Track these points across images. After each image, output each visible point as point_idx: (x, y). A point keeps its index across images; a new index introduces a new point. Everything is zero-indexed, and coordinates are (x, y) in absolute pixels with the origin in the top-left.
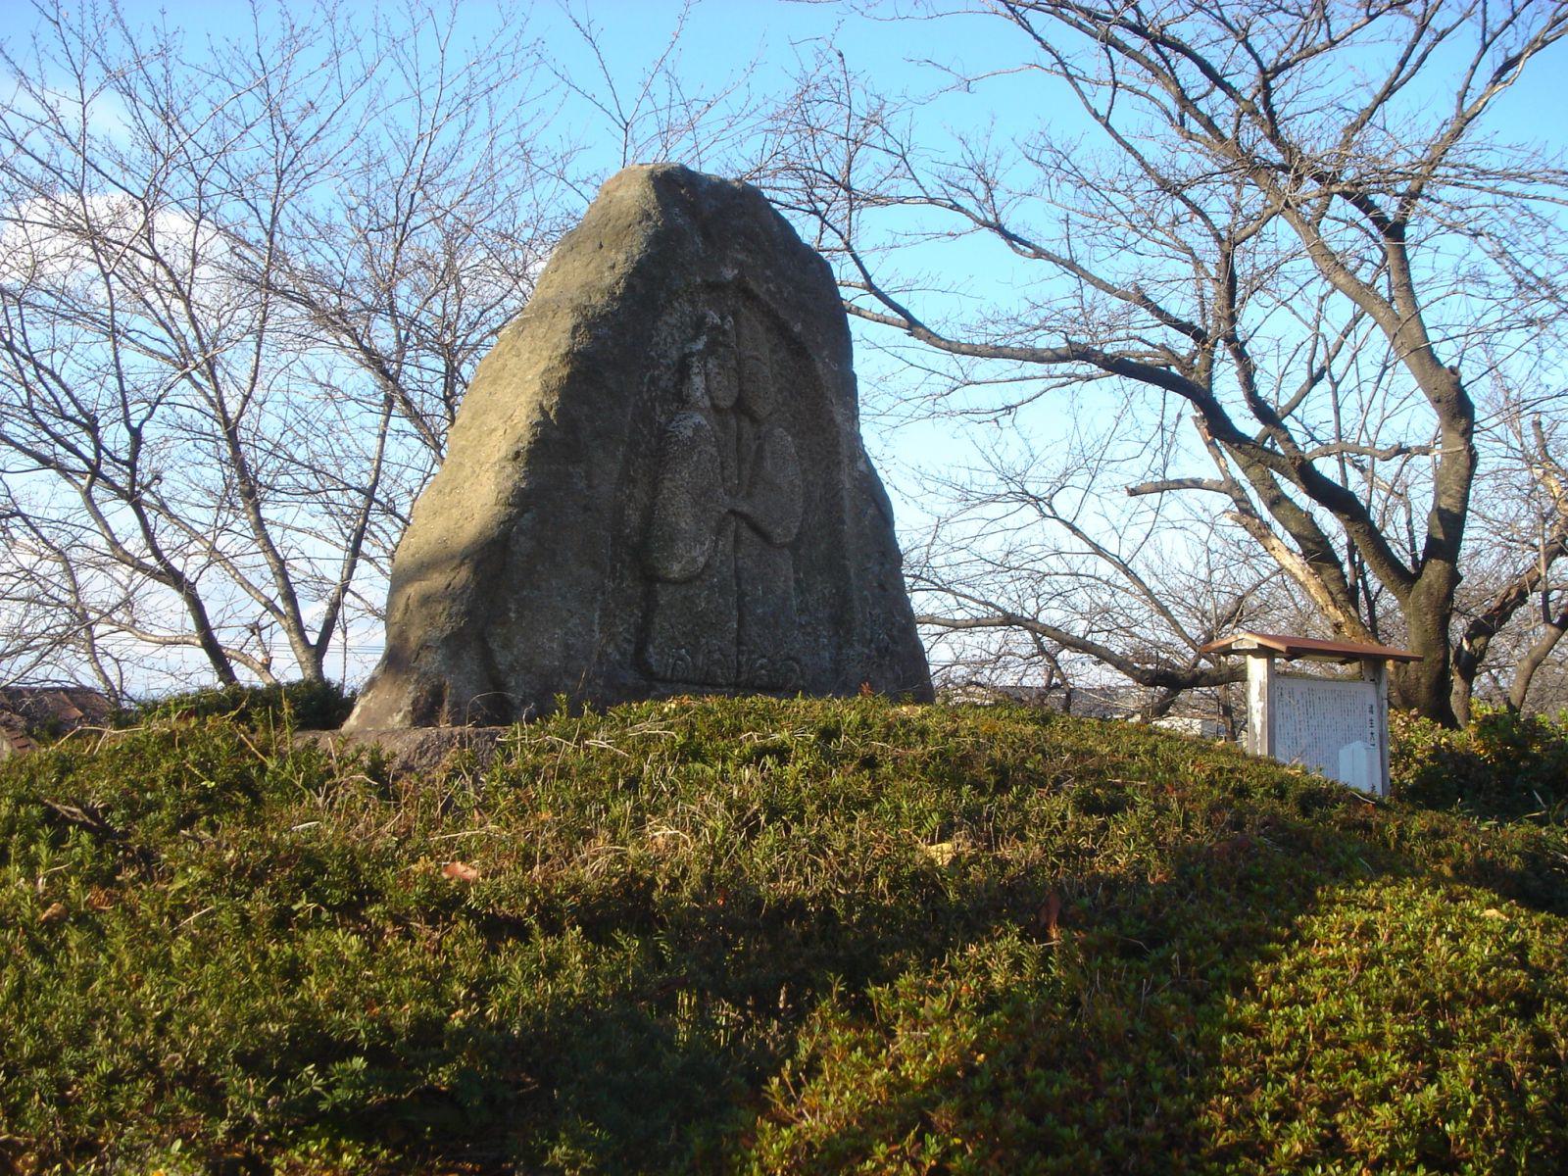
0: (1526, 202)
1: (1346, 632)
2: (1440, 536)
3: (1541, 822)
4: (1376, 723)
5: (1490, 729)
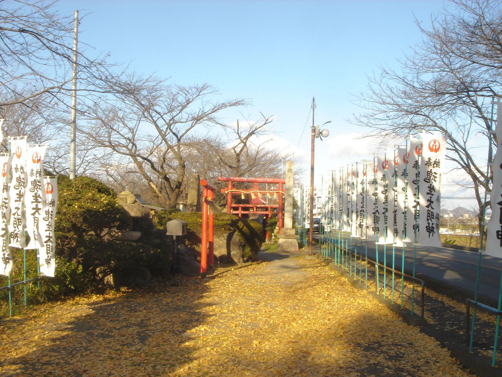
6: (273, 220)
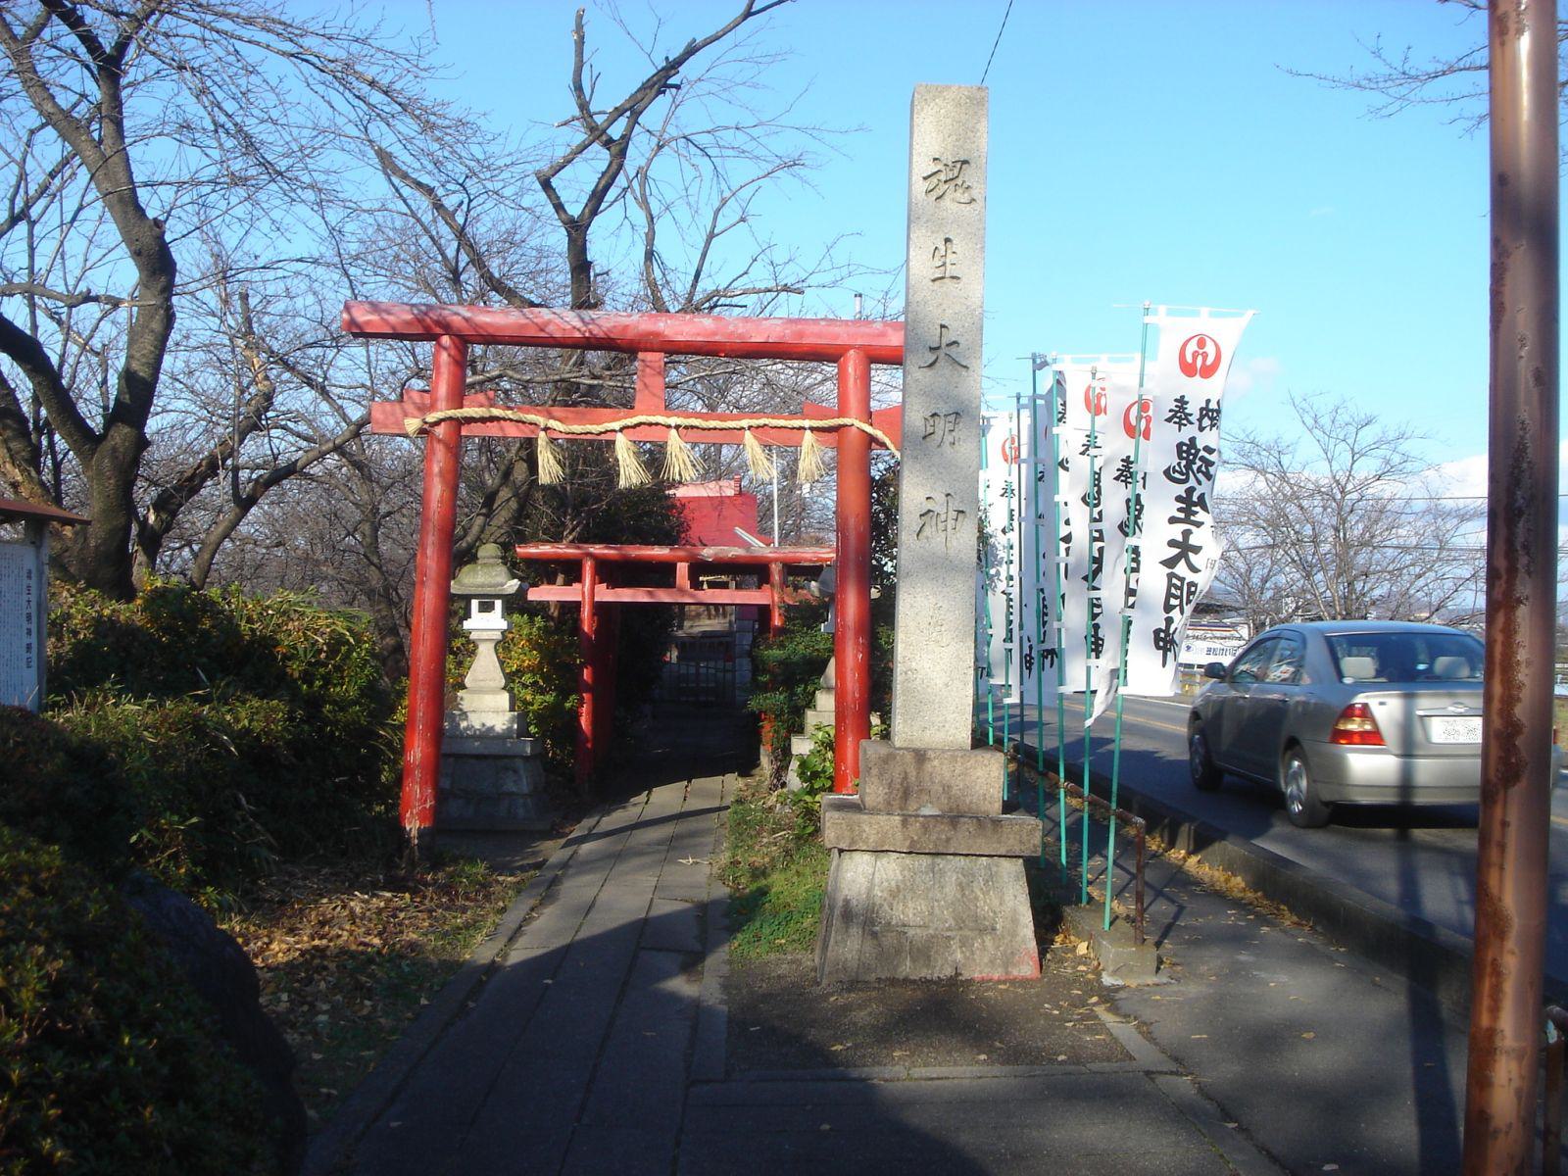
0: (239, 45)
1: (24, 492)
2: (127, 398)
3: (203, 700)
4: (34, 591)
5: (160, 602)
6: (800, 647)
